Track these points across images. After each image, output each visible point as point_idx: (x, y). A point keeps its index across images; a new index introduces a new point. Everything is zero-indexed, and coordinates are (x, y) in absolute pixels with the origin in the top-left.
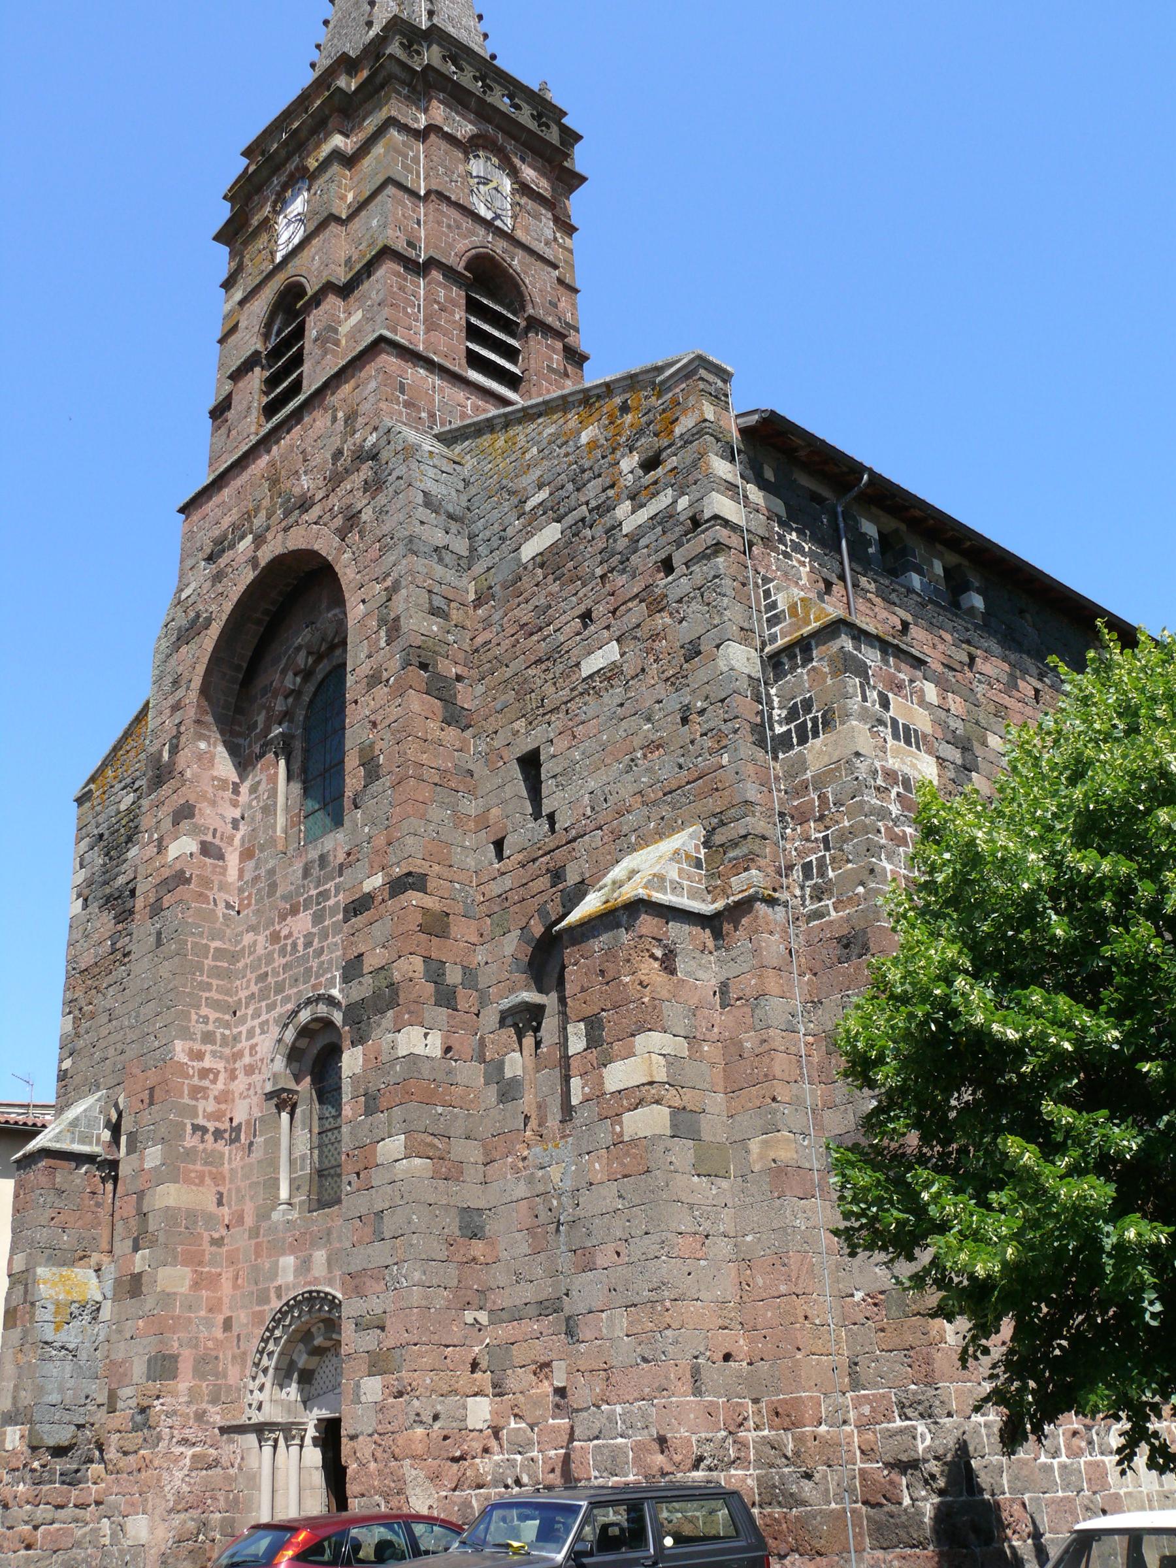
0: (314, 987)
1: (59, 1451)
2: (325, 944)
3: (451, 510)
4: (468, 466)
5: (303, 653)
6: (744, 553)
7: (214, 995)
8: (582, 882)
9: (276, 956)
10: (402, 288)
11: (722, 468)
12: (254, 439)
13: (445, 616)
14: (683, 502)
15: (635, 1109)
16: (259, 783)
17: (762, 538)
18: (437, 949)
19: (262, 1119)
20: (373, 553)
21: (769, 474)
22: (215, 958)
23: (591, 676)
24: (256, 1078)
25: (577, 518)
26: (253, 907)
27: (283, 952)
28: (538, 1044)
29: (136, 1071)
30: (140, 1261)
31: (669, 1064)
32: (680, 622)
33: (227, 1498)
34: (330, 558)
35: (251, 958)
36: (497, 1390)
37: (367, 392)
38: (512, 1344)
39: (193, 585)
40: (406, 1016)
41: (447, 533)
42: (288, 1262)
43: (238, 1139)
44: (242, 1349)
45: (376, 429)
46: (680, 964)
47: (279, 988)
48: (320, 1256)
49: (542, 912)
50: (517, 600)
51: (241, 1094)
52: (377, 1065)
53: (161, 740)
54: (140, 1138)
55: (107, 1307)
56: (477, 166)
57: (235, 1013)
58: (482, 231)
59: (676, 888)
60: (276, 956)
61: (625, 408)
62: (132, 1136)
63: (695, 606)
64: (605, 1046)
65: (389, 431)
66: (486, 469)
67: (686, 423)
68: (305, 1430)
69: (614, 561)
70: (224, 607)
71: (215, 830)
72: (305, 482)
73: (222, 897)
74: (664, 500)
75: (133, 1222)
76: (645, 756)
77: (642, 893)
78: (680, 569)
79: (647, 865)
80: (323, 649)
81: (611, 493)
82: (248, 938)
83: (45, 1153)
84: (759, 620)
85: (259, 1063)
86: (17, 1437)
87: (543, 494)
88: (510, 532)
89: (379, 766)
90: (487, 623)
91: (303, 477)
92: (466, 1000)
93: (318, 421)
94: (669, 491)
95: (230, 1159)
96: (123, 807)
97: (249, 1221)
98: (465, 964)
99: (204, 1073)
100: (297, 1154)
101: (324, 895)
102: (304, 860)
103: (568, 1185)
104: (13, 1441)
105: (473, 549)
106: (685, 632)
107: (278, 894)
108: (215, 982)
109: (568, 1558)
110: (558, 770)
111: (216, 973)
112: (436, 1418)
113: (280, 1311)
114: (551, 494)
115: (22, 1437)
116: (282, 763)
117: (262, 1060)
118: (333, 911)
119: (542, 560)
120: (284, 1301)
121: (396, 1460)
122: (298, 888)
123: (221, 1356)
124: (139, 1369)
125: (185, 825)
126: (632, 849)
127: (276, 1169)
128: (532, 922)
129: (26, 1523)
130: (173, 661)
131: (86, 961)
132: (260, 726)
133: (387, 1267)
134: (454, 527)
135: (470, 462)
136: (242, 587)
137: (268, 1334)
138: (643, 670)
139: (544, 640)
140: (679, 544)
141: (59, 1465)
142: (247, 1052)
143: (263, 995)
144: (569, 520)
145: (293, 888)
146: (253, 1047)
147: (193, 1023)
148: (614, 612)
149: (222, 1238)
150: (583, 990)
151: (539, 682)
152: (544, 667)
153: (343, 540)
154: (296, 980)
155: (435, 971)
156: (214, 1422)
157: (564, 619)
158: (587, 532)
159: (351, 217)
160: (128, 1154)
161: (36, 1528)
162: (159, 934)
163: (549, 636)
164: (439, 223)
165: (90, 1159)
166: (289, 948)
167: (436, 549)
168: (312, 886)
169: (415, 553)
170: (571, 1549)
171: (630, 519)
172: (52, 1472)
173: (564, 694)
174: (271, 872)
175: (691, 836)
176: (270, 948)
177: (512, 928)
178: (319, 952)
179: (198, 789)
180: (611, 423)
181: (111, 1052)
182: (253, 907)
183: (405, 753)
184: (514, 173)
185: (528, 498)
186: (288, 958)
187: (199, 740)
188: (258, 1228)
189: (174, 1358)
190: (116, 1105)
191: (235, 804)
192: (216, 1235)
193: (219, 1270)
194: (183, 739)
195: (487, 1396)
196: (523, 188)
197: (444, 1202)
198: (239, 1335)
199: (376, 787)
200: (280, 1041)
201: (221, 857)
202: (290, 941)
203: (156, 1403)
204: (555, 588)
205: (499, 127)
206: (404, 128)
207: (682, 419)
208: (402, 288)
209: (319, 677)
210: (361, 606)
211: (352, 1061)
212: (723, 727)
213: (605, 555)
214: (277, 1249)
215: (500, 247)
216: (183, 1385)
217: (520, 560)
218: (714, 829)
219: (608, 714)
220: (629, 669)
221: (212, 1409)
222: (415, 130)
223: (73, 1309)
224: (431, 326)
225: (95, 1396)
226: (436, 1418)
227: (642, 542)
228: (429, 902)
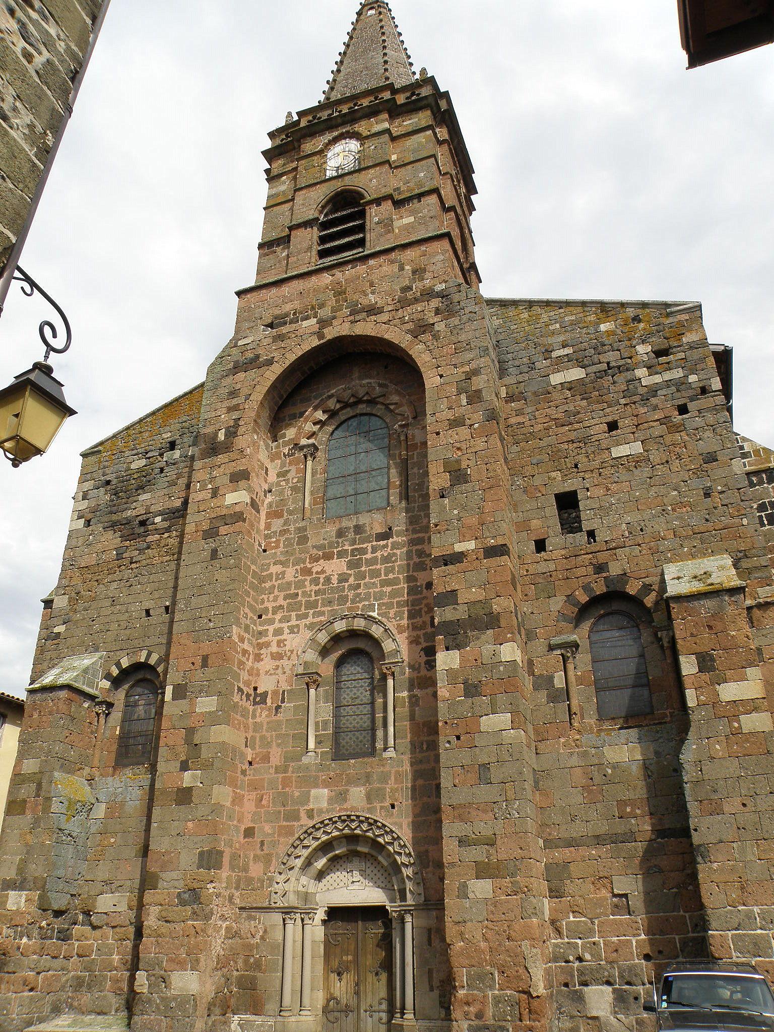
0: (349, 609)
1: (58, 913)
2: (362, 582)
15: (751, 713)
19: (290, 691)
26: (281, 549)
35: (279, 582)
38: (569, 863)
43: (264, 701)
44: (266, 851)
66: (512, 327)
69: (636, 398)
76: (673, 510)
86: (23, 901)
125: (242, 483)
129: (32, 970)
137: (298, 842)
141: (58, 923)
145: (326, 542)
157: (593, 422)
159: (396, 167)
161: (38, 973)
165: (92, 698)
172: (53, 929)
189: (220, 853)
214: (309, 781)
221: (237, 894)
225: (84, 873)
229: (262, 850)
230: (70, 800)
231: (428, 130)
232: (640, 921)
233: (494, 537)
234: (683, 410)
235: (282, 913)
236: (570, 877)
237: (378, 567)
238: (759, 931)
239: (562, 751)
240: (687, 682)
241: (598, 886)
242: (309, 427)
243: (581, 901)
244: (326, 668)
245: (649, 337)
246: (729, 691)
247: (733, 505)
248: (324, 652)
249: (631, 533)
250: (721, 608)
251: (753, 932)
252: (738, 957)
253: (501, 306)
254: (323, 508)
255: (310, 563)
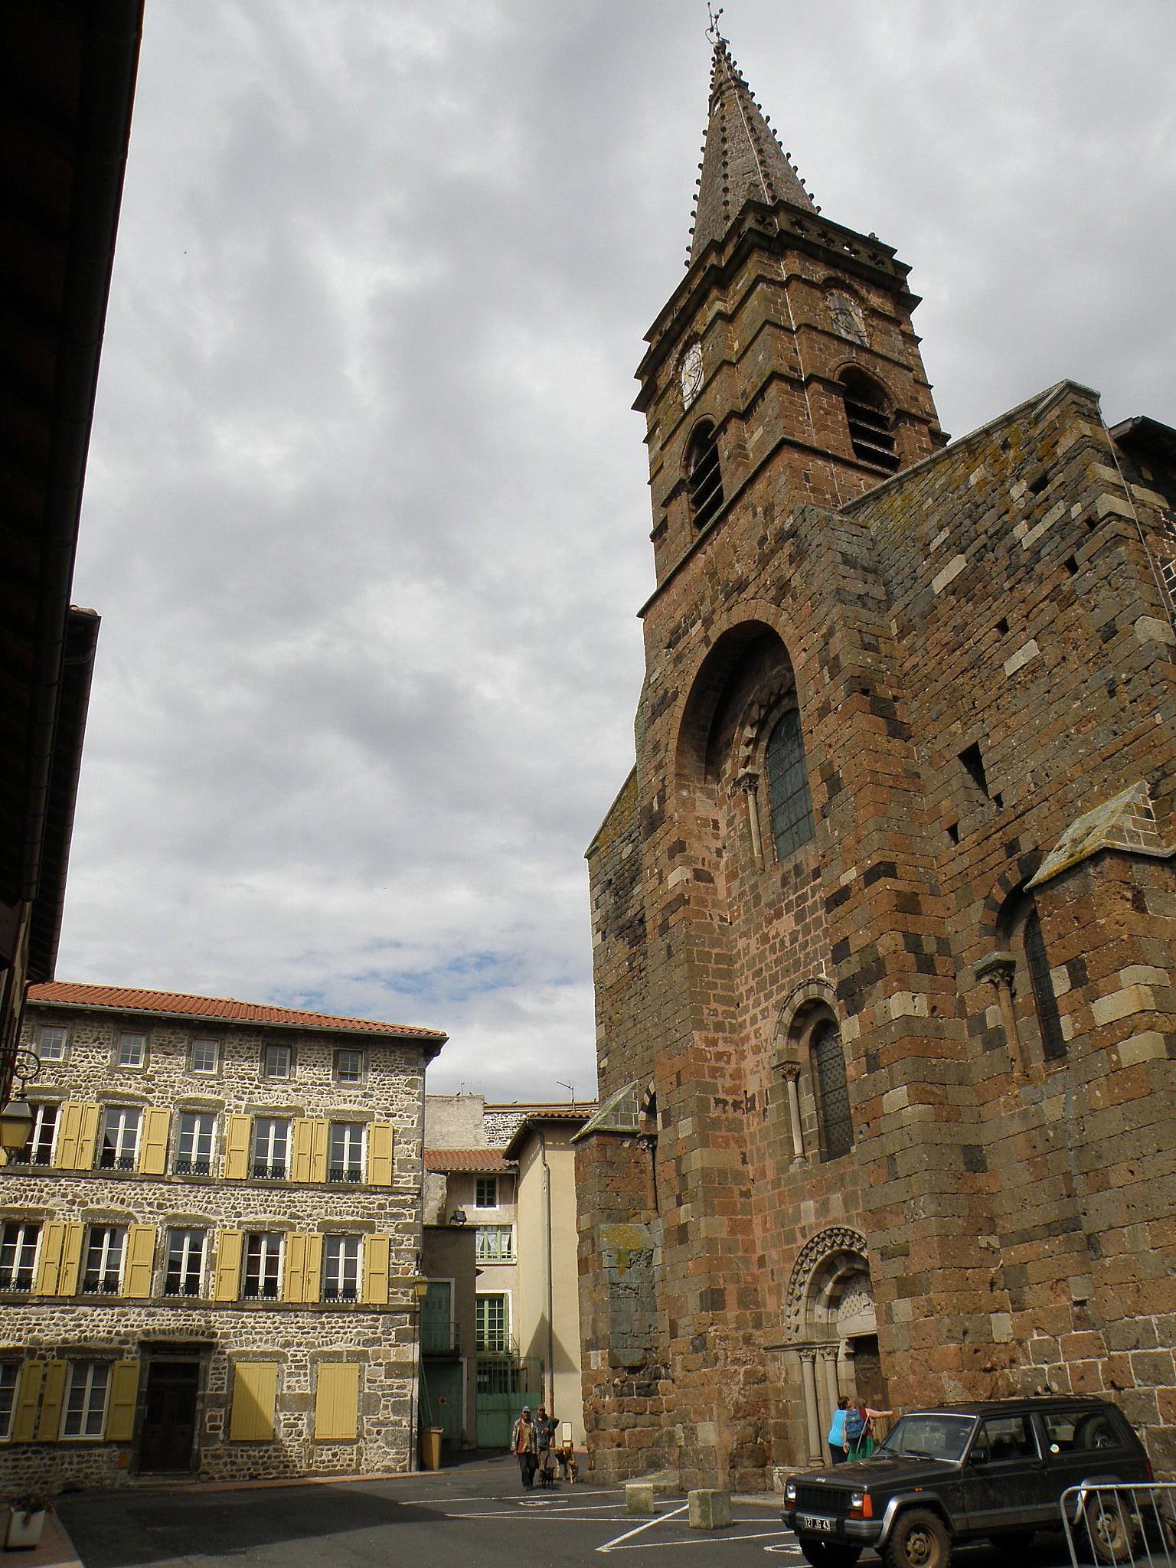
0: (805, 975)
1: (633, 1369)
2: (809, 937)
3: (866, 565)
4: (873, 529)
5: (756, 707)
6: (1141, 542)
7: (719, 991)
8: (1036, 849)
9: (767, 953)
10: (791, 403)
11: (1108, 474)
12: (690, 547)
13: (877, 650)
14: (1076, 510)
15: (1130, 1037)
16: (734, 817)
17: (1153, 528)
18: (914, 925)
19: (771, 1089)
20: (805, 611)
21: (1148, 476)
22: (717, 962)
23: (1015, 673)
24: (763, 1055)
25: (979, 546)
27: (773, 949)
28: (1013, 995)
29: (663, 1060)
30: (684, 1214)
31: (1156, 994)
32: (1093, 610)
33: (777, 1407)
34: (770, 623)
35: (747, 958)
36: (1016, 1306)
37: (778, 487)
38: (1026, 1263)
39: (659, 670)
40: (895, 984)
41: (866, 583)
42: (809, 1206)
43: (753, 1108)
44: (776, 1282)
45: (792, 512)
46: (1149, 904)
47: (774, 979)
48: (836, 1198)
49: (1002, 881)
50: (935, 626)
51: (751, 1071)
52: (874, 1029)
53: (650, 795)
54: (673, 1114)
55: (658, 1252)
56: (832, 302)
57: (738, 1005)
58: (847, 349)
59: (1134, 836)
60: (767, 953)
61: (1006, 446)
62: (666, 1114)
63: (1103, 593)
64: (1090, 984)
65: (803, 511)
67: (1066, 443)
68: (838, 1347)
69: (1020, 574)
70: (687, 681)
71: (703, 859)
72: (739, 568)
73: (715, 912)
74: (1058, 512)
75: (675, 1182)
76: (1078, 731)
77: (1105, 842)
78: (1083, 565)
79: (1101, 820)
80: (772, 700)
81: (1006, 518)
82: (741, 943)
83: (596, 1132)
84: (1165, 596)
85: (764, 1044)
87: (945, 534)
88: (920, 572)
89: (839, 779)
90: (912, 651)
91: (737, 565)
92: (942, 965)
93: (740, 519)
94: (1061, 503)
95: (748, 1124)
96: (624, 856)
97: (771, 1174)
98: (938, 935)
99: (719, 1056)
100: (804, 1116)
101: (803, 898)
102: (781, 872)
103: (1072, 1114)
104: (596, 1363)
105: (889, 594)
106: (1100, 617)
107: (762, 904)
108: (719, 981)
109: (965, 1464)
110: (998, 758)
111: (719, 974)
112: (965, 1333)
113: (806, 1247)
114: (951, 533)
115: (603, 1359)
116: (751, 798)
117: (766, 1040)
118: (814, 909)
119: (952, 589)
120: (809, 1239)
121: (934, 1372)
122: (779, 896)
123: (759, 1289)
124: (693, 1302)
125: (678, 858)
126: (1080, 812)
127: (789, 1130)
128: (994, 891)
129: (616, 1427)
130: (650, 732)
131: (611, 979)
132: (729, 772)
133: (904, 1202)
134: (870, 578)
135: (874, 525)
136: (699, 663)
137: (798, 1267)
138: (1064, 658)
139: (966, 653)
140: (1079, 545)
141: (635, 1380)
142: (752, 1036)
143: (761, 986)
144: (972, 549)
145: (775, 896)
146: (757, 1031)
147: (706, 1016)
148: (1027, 616)
149: (749, 1191)
150: (1060, 937)
151: (967, 688)
152: (970, 674)
153: (778, 606)
154: (787, 971)
155: (913, 943)
156: (760, 1344)
157: (982, 631)
158: (991, 555)
159: (739, 360)
160: (664, 1127)
161: (623, 1430)
162: (669, 947)
163: (970, 649)
164: (812, 348)
165: (632, 1135)
166: (778, 945)
167: (860, 597)
168: (791, 892)
169: (842, 602)
170: (968, 1457)
171: (1025, 535)
172: (630, 1386)
173: (993, 693)
174: (754, 887)
175: (1139, 790)
176: (761, 948)
177: (976, 899)
178: (805, 945)
179: (686, 828)
180: (995, 462)
181: (639, 1049)
182: (743, 917)
183: (862, 764)
184: (862, 301)
185: (931, 541)
186: (778, 954)
187: (681, 789)
188: (779, 1179)
189: (721, 1292)
190: (648, 1091)
191: (717, 837)
192: (744, 1189)
193: (749, 1217)
194: (668, 790)
195: (1008, 1312)
196: (873, 313)
197: (948, 1142)
198: (772, 1270)
199: (840, 797)
200: (779, 1022)
201: (711, 880)
202: (778, 940)
203: (710, 1329)
204: (969, 607)
205: (844, 270)
206: (771, 282)
207: (1062, 441)
208: (791, 403)
209: (772, 724)
210: (803, 654)
211: (850, 1028)
212: (1151, 691)
213: (1011, 571)
214: (798, 1195)
215: (863, 360)
216: (732, 1313)
217: (933, 592)
218: (1158, 781)
219: (1037, 701)
220: (1050, 660)
221: (756, 1333)
222: (779, 282)
223: (631, 1256)
224: (821, 427)
226: (965, 1333)
227: (1043, 552)
228: (901, 885)
229: (774, 1280)
230: (619, 1252)
231: (758, 284)
232: (1102, 1337)
233: (869, 857)
234: (1072, 566)
235: (797, 1350)
236: (1028, 1284)
237: (819, 914)
238: (1160, 1349)
239: (1003, 1114)
240: (1062, 1005)
241: (1059, 1291)
242: (744, 751)
243: (1042, 1314)
244: (802, 1050)
245: (1023, 468)
246: (1107, 1009)
247: (1143, 697)
248: (794, 1033)
249: (1037, 785)
250: (1086, 886)
251: (1152, 1351)
252: (1140, 1386)
253: (875, 499)
254: (774, 850)
255: (766, 927)
